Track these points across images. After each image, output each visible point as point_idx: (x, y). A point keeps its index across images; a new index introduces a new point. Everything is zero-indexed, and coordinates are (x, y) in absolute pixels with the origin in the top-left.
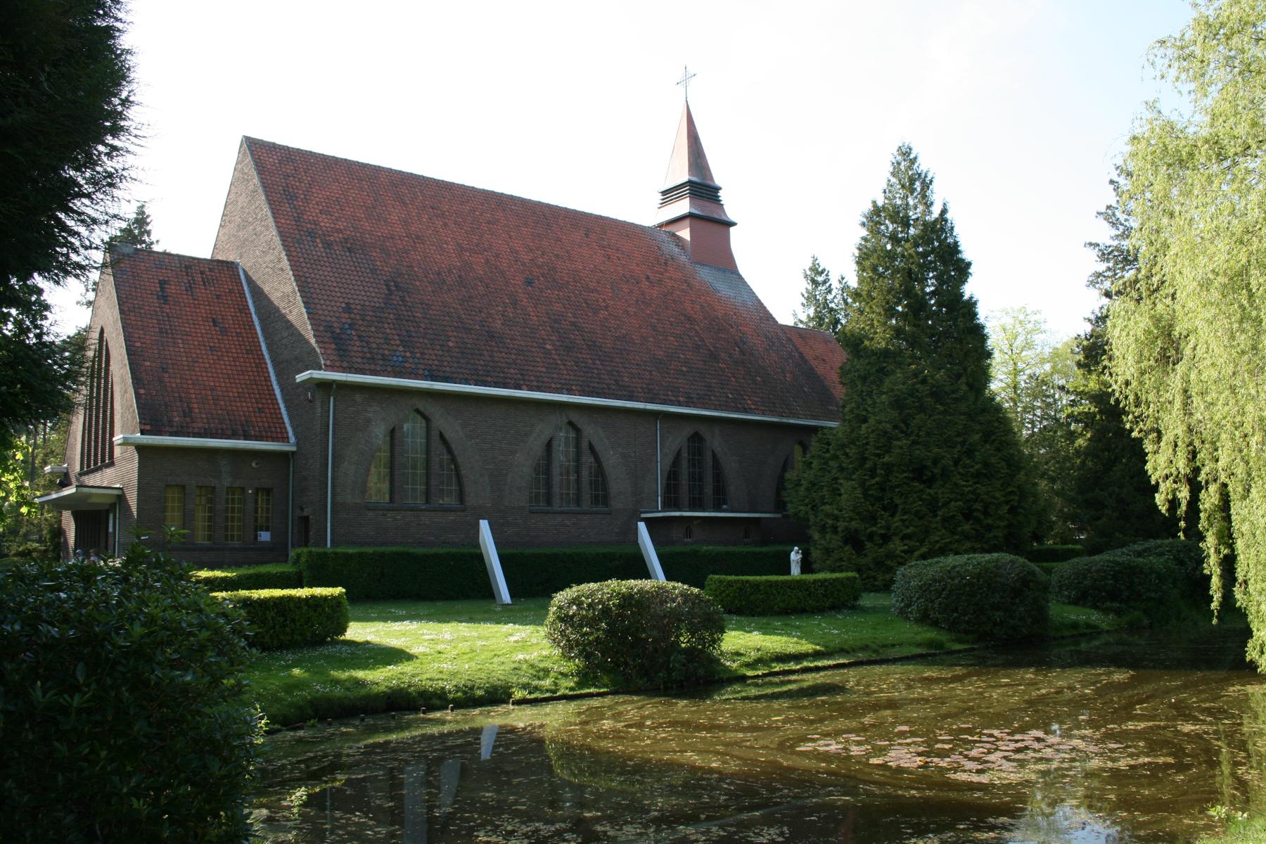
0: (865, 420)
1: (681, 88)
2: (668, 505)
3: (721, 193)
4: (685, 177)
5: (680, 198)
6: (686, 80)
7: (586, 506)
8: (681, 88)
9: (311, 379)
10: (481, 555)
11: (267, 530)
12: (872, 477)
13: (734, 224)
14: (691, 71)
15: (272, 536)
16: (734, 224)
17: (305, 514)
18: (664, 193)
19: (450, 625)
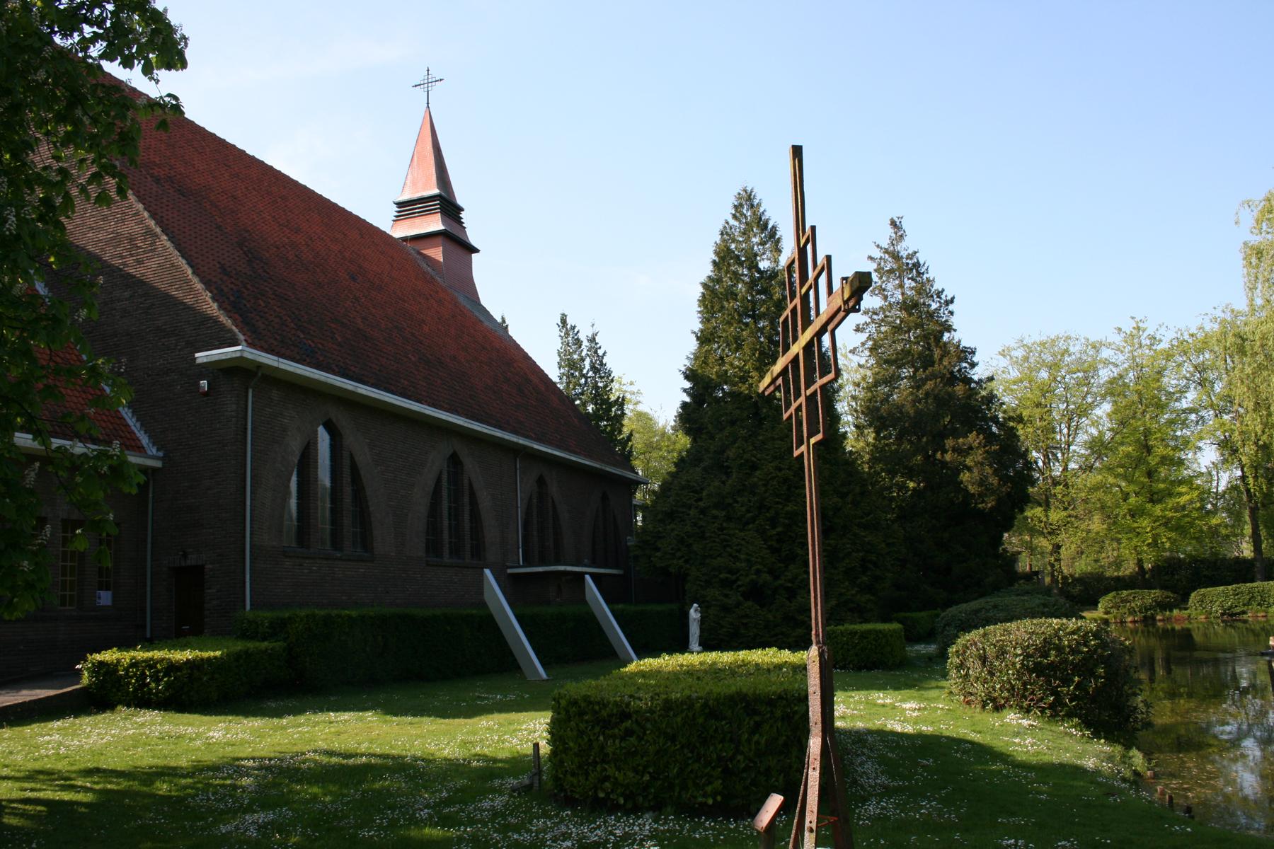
0: (754, 467)
1: (421, 93)
2: (528, 562)
3: (463, 215)
4: (436, 191)
5: (428, 212)
6: (428, 83)
7: (447, 559)
8: (421, 93)
9: (241, 358)
10: (491, 617)
11: (107, 589)
12: (774, 527)
13: (476, 251)
14: (435, 74)
15: (114, 597)
16: (476, 251)
17: (192, 560)
18: (400, 204)
19: (301, 719)
